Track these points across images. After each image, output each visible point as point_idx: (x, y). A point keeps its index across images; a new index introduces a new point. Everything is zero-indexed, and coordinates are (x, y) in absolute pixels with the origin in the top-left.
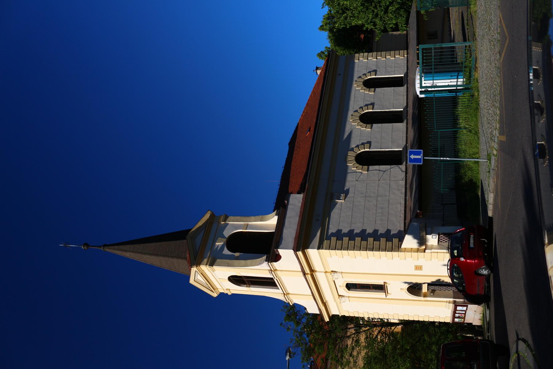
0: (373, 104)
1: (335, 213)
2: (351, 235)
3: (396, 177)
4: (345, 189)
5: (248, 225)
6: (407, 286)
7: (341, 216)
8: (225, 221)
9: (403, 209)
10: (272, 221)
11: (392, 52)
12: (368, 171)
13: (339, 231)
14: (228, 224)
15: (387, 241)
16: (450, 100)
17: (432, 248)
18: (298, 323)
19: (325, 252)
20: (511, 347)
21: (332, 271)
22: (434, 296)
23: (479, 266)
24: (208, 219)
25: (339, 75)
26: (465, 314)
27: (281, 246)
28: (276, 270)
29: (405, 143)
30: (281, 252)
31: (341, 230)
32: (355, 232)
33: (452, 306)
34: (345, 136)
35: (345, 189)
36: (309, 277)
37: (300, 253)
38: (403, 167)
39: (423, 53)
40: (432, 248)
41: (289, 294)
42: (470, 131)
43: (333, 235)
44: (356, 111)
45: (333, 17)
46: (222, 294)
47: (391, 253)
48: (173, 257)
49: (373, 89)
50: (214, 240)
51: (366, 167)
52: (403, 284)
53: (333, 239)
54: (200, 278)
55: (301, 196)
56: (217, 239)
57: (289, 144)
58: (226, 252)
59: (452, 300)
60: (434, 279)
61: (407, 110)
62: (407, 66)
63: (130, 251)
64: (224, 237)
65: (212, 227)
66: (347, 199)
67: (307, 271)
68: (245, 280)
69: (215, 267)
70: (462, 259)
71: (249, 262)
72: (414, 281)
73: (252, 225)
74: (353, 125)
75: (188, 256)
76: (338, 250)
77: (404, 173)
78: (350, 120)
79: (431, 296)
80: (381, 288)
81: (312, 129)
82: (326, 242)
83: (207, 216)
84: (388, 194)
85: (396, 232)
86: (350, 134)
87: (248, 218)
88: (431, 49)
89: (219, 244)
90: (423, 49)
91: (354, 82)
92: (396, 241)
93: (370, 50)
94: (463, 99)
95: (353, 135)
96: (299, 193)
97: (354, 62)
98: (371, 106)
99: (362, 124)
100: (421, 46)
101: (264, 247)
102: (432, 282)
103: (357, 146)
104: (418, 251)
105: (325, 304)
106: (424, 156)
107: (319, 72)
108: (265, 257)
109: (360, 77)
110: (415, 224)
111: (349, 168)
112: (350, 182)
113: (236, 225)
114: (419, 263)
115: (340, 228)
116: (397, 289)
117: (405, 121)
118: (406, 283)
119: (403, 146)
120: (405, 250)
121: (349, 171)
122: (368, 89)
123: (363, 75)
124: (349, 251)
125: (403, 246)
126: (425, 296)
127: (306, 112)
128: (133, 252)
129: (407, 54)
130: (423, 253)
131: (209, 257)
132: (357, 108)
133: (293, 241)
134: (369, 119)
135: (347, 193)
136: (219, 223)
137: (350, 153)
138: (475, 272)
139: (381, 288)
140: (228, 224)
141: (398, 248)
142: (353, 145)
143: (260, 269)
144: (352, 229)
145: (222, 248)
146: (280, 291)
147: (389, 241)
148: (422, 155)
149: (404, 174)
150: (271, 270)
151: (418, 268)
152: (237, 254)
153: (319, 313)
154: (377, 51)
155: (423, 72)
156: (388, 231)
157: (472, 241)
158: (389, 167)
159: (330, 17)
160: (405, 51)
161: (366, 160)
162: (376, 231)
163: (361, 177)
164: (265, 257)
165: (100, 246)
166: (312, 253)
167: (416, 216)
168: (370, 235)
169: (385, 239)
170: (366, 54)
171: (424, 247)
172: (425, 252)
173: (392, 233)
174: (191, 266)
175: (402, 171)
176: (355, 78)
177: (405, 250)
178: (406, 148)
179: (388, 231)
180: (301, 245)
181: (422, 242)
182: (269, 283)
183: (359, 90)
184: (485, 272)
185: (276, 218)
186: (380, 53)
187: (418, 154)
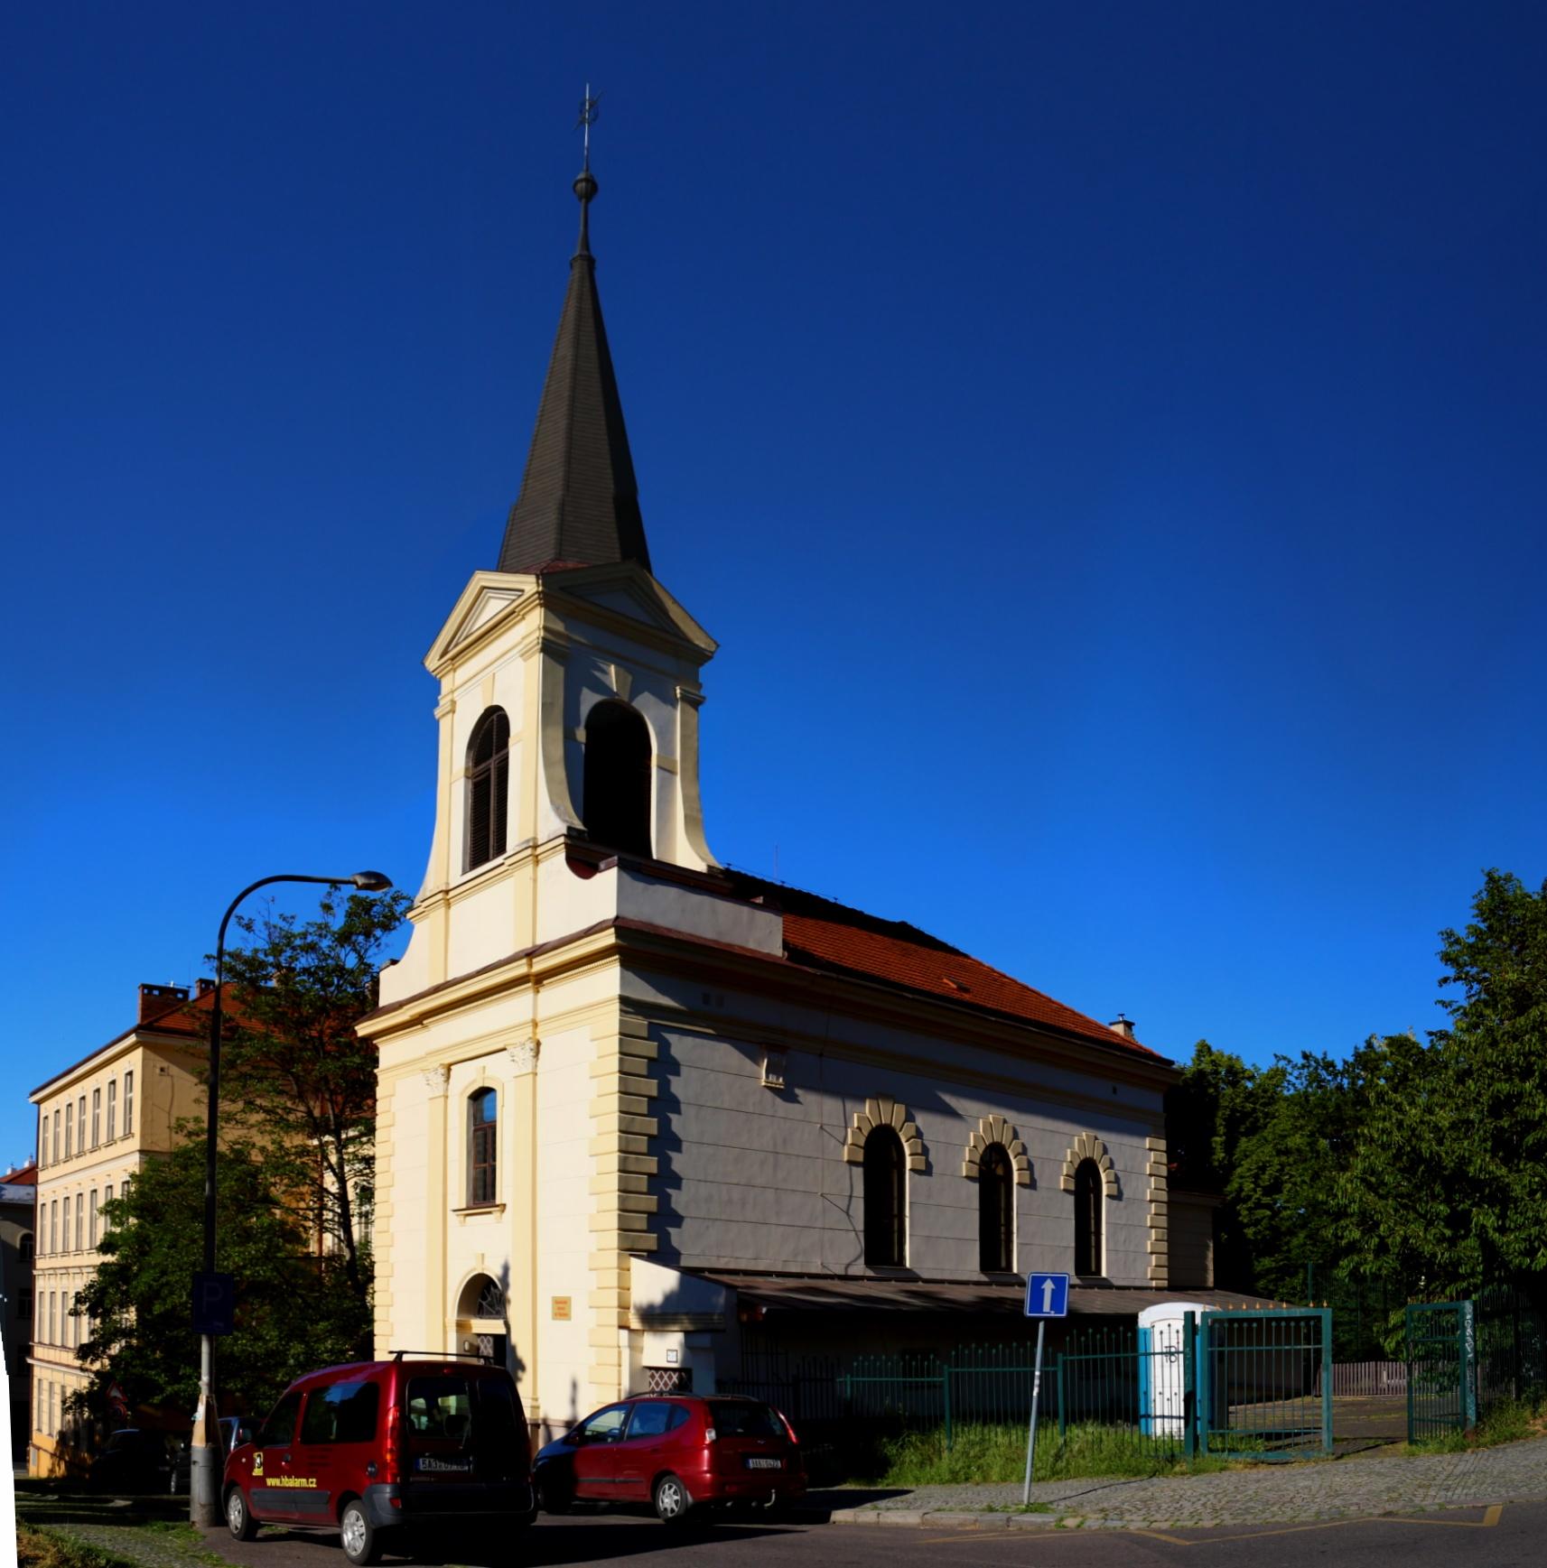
0: (1031, 1185)
1: (725, 1055)
2: (664, 1105)
3: (835, 1250)
4: (797, 1091)
5: (673, 773)
6: (494, 1272)
7: (719, 1074)
8: (684, 698)
9: (743, 1265)
10: (686, 854)
11: (1164, 1247)
12: (851, 1163)
13: (675, 1067)
14: (674, 706)
15: (650, 1214)
16: (1126, 1405)
17: (635, 1348)
18: (344, 938)
19: (611, 1019)
21: (538, 1044)
23: (690, 1483)
24: (689, 641)
25: (1115, 1091)
27: (626, 877)
28: (537, 862)
29: (925, 1275)
30: (608, 879)
31: (677, 1073)
32: (673, 1117)
34: (948, 1098)
35: (797, 1091)
36: (520, 969)
37: (608, 938)
38: (859, 1268)
39: (1307, 1319)
40: (635, 1348)
41: (448, 905)
42: (1058, 1457)
43: (664, 1046)
44: (1016, 1136)
45: (1234, 1084)
46: (435, 685)
47: (615, 1225)
49: (1072, 1187)
51: (860, 1158)
52: (502, 1262)
53: (651, 1048)
54: (494, 607)
55: (777, 950)
56: (630, 671)
57: (903, 924)
58: (589, 700)
60: (523, 1352)
61: (1012, 1285)
62: (1128, 1288)
63: (576, 357)
64: (635, 693)
66: (769, 1094)
67: (541, 964)
68: (492, 763)
69: (537, 660)
70: (710, 1436)
71: (561, 773)
72: (511, 1294)
73: (671, 784)
74: (981, 1122)
75: (570, 565)
76: (621, 1061)
77: (842, 1272)
78: (993, 1114)
80: (483, 1192)
81: (967, 997)
82: (640, 1024)
83: (701, 641)
84: (784, 1221)
85: (675, 1242)
86: (953, 1114)
88: (1319, 1341)
89: (612, 675)
90: (1319, 1319)
91: (1092, 1133)
92: (651, 1241)
93: (1174, 1182)
94: (1112, 1436)
95: (949, 1123)
96: (786, 945)
97: (1143, 1135)
98: (1027, 1181)
99: (981, 1149)
101: (608, 824)
102: (513, 1349)
103: (919, 1134)
104: (623, 1307)
105: (418, 1021)
106: (1047, 1320)
107: (1119, 1029)
108: (579, 825)
109: (1105, 1151)
110: (722, 1300)
111: (858, 1106)
112: (817, 1106)
113: (668, 733)
114: (577, 1309)
115: (684, 1070)
116: (483, 1245)
117: (984, 1278)
118: (506, 1269)
119: (917, 1271)
120: (624, 1270)
121: (849, 1105)
122: (1072, 1172)
123: (1112, 1162)
124: (616, 1096)
125: (637, 1265)
126: (461, 1326)
127: (1003, 984)
128: (575, 370)
129: (1158, 1289)
130: (615, 1322)
131: (568, 639)
132: (1023, 1138)
133: (644, 918)
134: (993, 1172)
135: (787, 1095)
136: (678, 681)
137: (899, 1110)
138: (669, 1473)
139: (483, 1192)
141: (629, 1249)
142: (922, 1119)
143: (536, 805)
144: (683, 1107)
145: (599, 687)
146: (456, 877)
147: (651, 1224)
148: (1053, 1314)
149: (839, 1271)
150: (535, 847)
151: (562, 1308)
152: (581, 735)
153: (382, 1003)
154: (1169, 1203)
155: (1214, 1321)
156: (677, 1220)
157: (764, 1463)
158: (860, 1226)
159: (1235, 1074)
160: (1165, 1283)
161: (881, 1160)
162: (676, 1181)
163: (833, 1142)
164: (579, 825)
166: (608, 980)
167: (745, 1302)
168: (665, 1163)
169: (654, 1208)
170: (1164, 1171)
171: (635, 1324)
172: (621, 1327)
173: (671, 1230)
174: (544, 576)
175: (848, 1265)
176: (1104, 1137)
177: (624, 1270)
178: (912, 1277)
179: (677, 1220)
180: (637, 946)
181: (655, 1318)
182: (486, 837)
183: (1071, 1146)
184: (669, 1500)
185: (701, 867)
186: (1164, 1211)
187: (1056, 1304)
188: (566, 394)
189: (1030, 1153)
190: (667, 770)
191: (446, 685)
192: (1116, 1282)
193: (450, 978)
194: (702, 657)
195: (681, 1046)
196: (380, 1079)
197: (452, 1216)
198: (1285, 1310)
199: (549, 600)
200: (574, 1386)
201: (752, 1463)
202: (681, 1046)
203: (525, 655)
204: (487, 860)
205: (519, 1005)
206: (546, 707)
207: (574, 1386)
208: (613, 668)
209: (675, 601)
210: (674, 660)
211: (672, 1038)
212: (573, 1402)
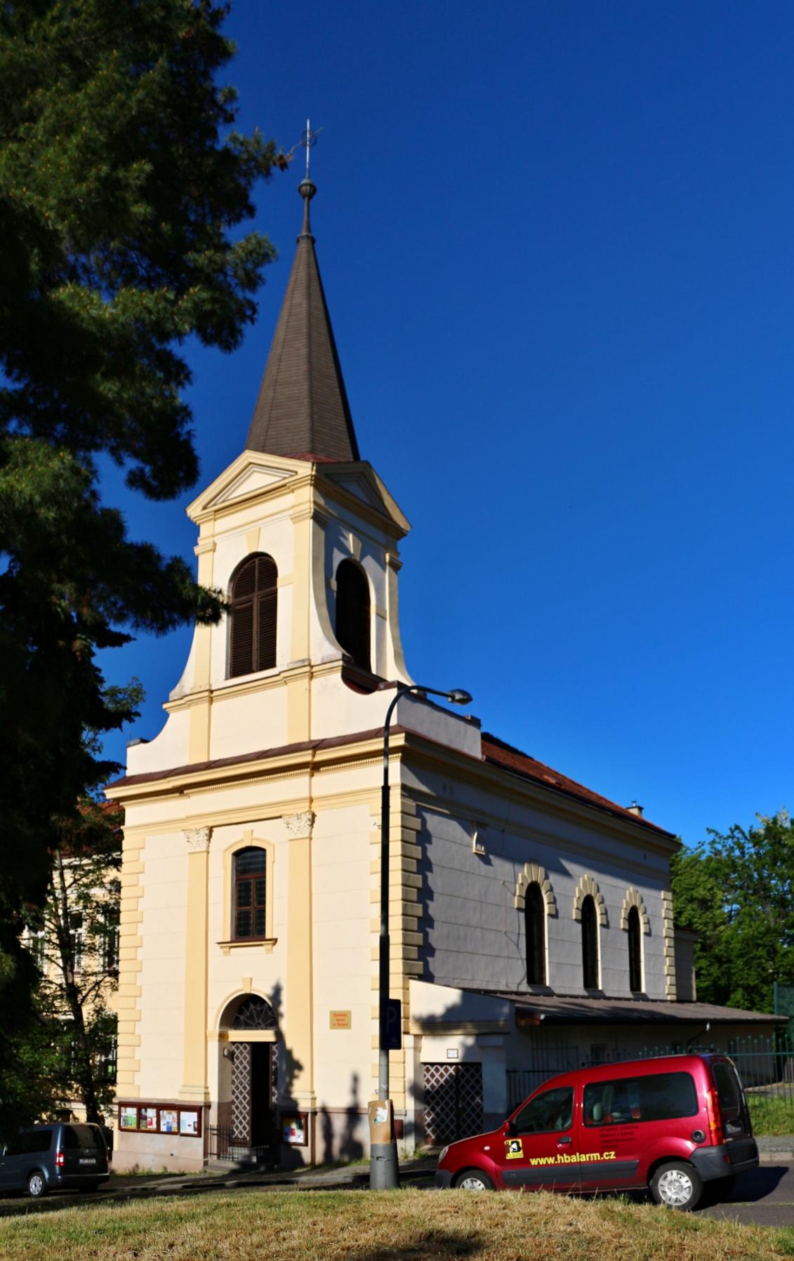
3: (513, 978)
4: (491, 857)
6: (264, 992)
12: (519, 909)
20: (394, 1236)
21: (314, 816)
22: (222, 1057)
26: (169, 1133)
33: (199, 1099)
35: (491, 857)
36: (306, 757)
38: (525, 987)
43: (424, 822)
48: (312, 415)
50: (361, 532)
52: (273, 983)
54: (257, 481)
56: (359, 538)
58: (338, 557)
59: (214, 1098)
64: (363, 556)
65: (384, 534)
66: (476, 858)
67: (322, 756)
79: (221, 1049)
82: (412, 804)
83: (402, 522)
84: (486, 952)
86: (566, 873)
87: (395, 620)
89: (351, 541)
92: (419, 967)
100: (236, 1035)
105: (180, 790)
107: (635, 812)
110: (506, 1010)
112: (501, 866)
113: (382, 591)
118: (277, 990)
121: (517, 867)
126: (222, 1036)
128: (310, 313)
129: (672, 1002)
135: (485, 859)
137: (541, 870)
140: (384, 570)
142: (554, 878)
145: (344, 549)
158: (524, 956)
160: (674, 998)
165: (309, 229)
174: (319, 465)
188: (305, 330)
189: (606, 902)
190: (381, 616)
191: (205, 530)
192: (651, 997)
193: (213, 758)
194: (400, 533)
195: (433, 822)
196: (125, 834)
197: (214, 950)
198: (769, 1017)
199: (318, 483)
200: (356, 1079)
201: (81, 1161)
202: (433, 822)
203: (296, 519)
204: (251, 671)
205: (297, 785)
206: (315, 559)
207: (356, 1079)
208: (351, 536)
209: (389, 493)
210: (384, 534)
211: (427, 816)
212: (355, 1091)
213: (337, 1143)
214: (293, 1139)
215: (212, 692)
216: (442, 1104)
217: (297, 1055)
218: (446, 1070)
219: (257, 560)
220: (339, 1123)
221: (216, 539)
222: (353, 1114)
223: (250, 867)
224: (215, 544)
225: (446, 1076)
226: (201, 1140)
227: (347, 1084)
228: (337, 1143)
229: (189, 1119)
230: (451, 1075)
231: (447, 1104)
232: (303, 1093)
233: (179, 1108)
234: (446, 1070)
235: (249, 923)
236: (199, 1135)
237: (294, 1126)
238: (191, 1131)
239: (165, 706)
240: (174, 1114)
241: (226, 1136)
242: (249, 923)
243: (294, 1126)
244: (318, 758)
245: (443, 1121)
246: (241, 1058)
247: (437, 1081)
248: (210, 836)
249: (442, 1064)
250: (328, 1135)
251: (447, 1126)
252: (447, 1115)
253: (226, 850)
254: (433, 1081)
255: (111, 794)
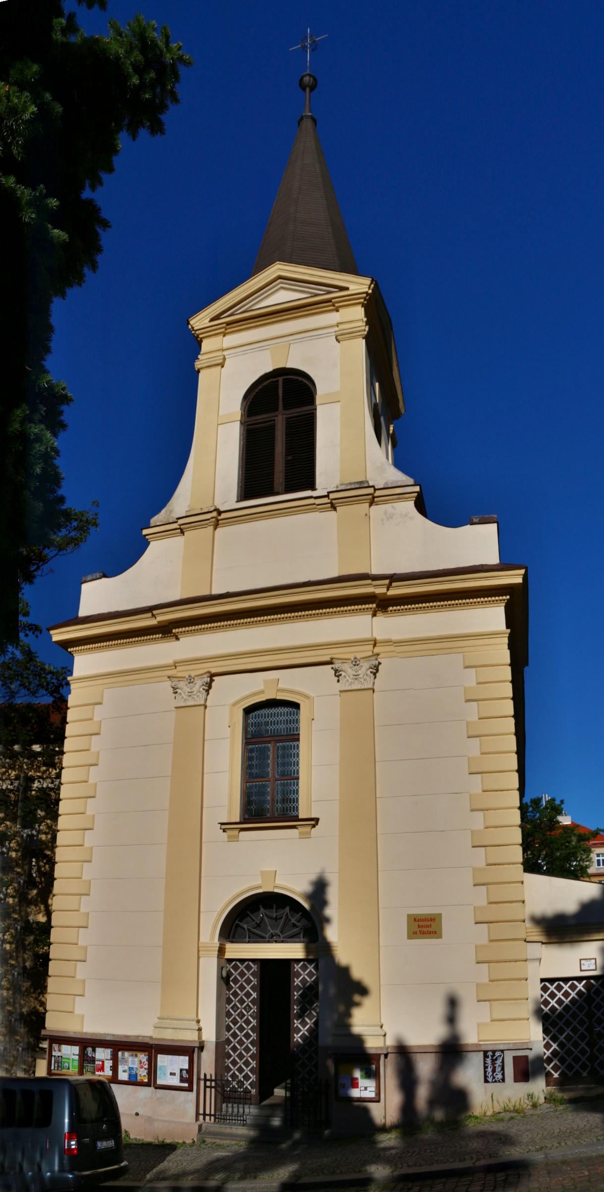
6: (297, 887)
33: (189, 1037)
52: (313, 877)
54: (283, 297)
59: (210, 1035)
67: (397, 590)
83: (403, 411)
118: (320, 888)
126: (221, 951)
191: (206, 345)
200: (453, 1003)
207: (453, 1003)
212: (451, 1019)
213: (423, 1093)
214: (355, 1093)
215: (220, 513)
216: (568, 1031)
217: (357, 973)
218: (573, 987)
219: (281, 379)
220: (425, 1067)
221: (225, 353)
222: (451, 1052)
223: (270, 733)
224: (224, 359)
225: (573, 994)
226: (193, 1095)
227: (439, 1009)
228: (423, 1093)
229: (171, 1067)
230: (580, 993)
231: (575, 1030)
232: (376, 1023)
233: (152, 1049)
234: (573, 987)
235: (268, 801)
236: (190, 1089)
237: (357, 1074)
238: (175, 1081)
239: (145, 532)
240: (143, 1057)
241: (226, 1093)
242: (268, 801)
243: (357, 1074)
244: (392, 592)
245: (569, 1053)
246: (242, 981)
247: (560, 1002)
248: (209, 686)
249: (566, 980)
250: (407, 1081)
251: (577, 1059)
252: (576, 1045)
253: (235, 704)
254: (553, 1003)
255: (58, 635)
